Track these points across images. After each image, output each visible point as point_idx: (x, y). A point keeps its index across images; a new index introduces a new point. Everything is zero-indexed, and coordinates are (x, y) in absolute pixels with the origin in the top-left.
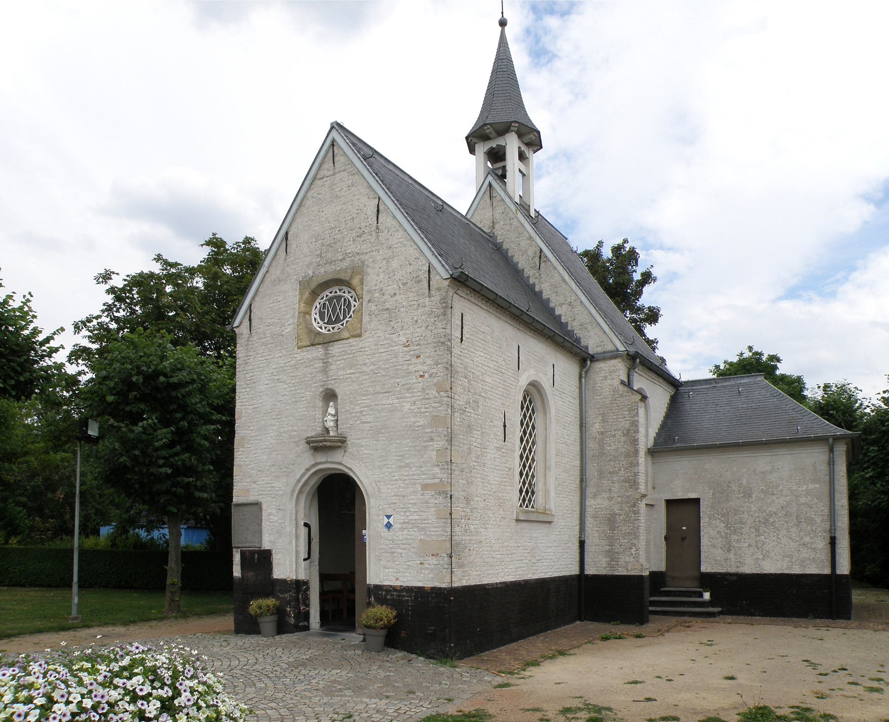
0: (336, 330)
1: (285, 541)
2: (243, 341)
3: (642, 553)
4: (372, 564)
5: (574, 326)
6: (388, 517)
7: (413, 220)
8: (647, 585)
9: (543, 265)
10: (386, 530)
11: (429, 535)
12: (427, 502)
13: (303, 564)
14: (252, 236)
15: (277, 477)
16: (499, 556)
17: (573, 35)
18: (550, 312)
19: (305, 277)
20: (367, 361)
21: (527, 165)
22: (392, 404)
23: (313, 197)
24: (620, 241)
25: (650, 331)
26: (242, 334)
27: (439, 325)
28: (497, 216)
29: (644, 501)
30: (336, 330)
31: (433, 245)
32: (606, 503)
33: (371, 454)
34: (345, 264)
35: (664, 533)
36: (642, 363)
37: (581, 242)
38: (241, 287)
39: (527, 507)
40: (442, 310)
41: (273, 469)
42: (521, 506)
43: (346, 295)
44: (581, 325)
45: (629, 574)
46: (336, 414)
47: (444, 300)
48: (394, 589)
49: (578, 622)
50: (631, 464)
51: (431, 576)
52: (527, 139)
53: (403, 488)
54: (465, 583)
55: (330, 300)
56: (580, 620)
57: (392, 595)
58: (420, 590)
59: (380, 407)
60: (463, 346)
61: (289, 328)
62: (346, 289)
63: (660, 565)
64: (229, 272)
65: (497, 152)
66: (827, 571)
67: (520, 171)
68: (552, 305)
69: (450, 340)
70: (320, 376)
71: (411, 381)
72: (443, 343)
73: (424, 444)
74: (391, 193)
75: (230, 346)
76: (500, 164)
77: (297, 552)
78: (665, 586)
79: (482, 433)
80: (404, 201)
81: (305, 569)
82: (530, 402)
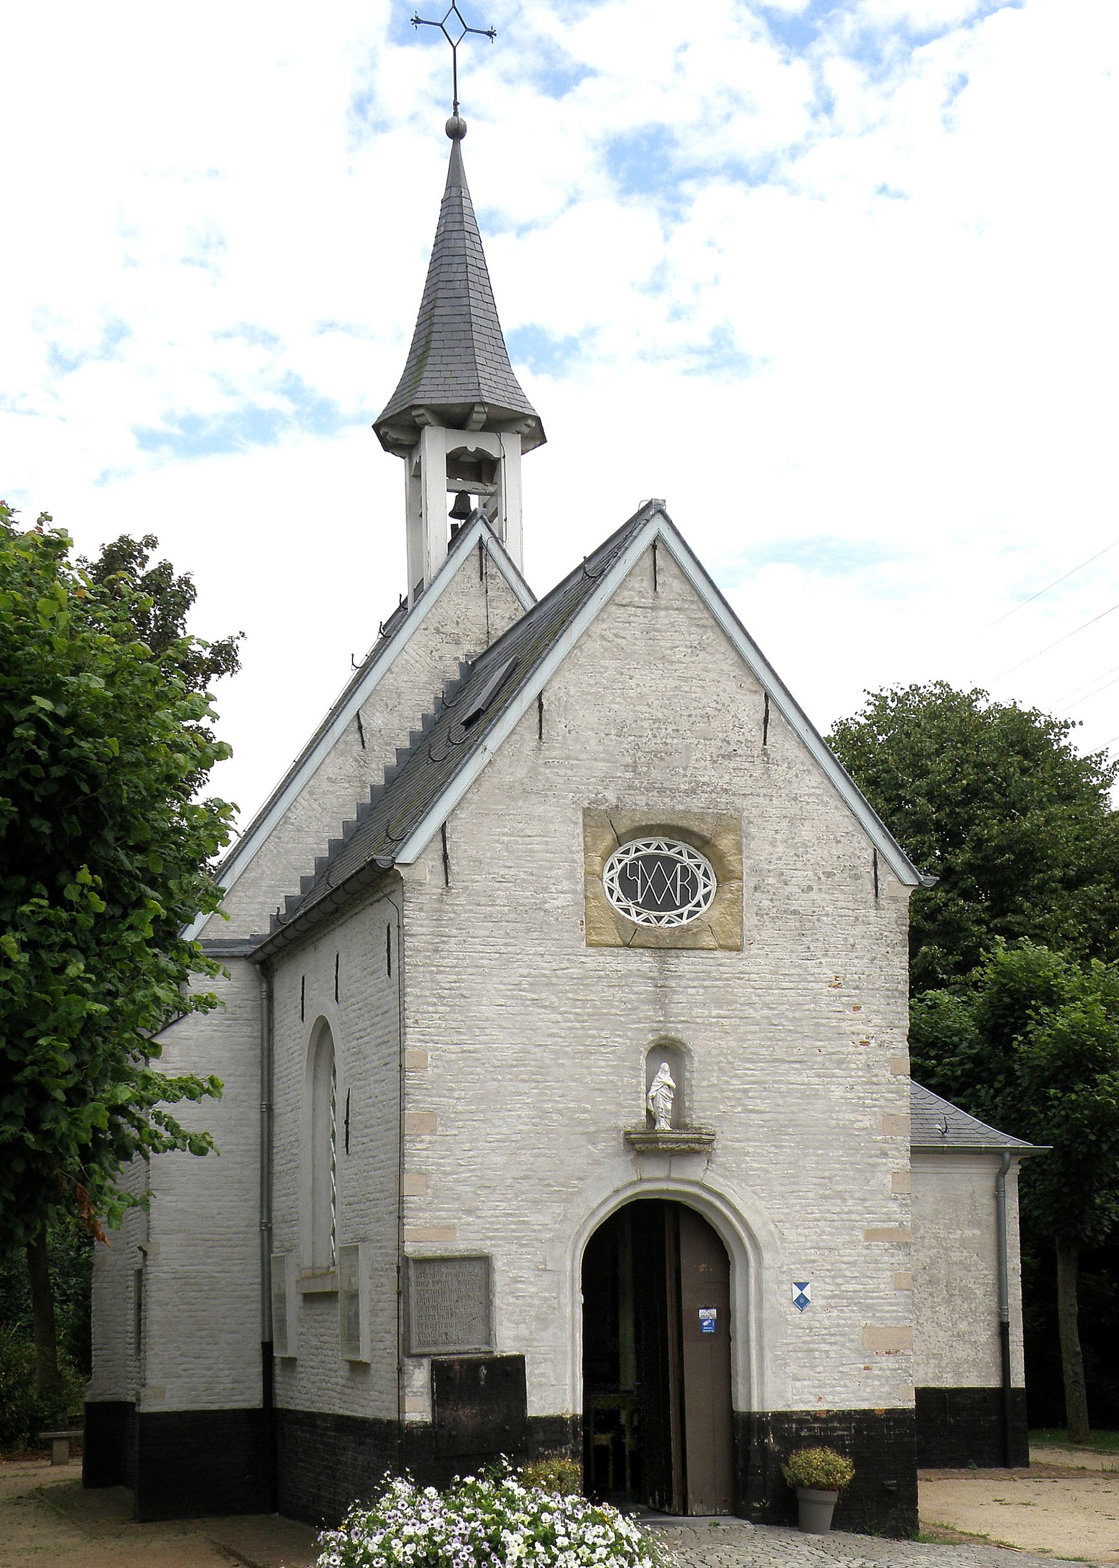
6: (801, 1286)
10: (794, 1309)
11: (880, 1319)
12: (876, 1262)
15: (535, 1202)
20: (755, 999)
22: (809, 1084)
23: (603, 637)
33: (768, 1172)
41: (525, 1185)
48: (815, 1417)
51: (886, 1389)
53: (830, 1234)
55: (649, 860)
57: (810, 1429)
59: (783, 1088)
66: (994, 1383)
70: (648, 1011)
73: (870, 1161)
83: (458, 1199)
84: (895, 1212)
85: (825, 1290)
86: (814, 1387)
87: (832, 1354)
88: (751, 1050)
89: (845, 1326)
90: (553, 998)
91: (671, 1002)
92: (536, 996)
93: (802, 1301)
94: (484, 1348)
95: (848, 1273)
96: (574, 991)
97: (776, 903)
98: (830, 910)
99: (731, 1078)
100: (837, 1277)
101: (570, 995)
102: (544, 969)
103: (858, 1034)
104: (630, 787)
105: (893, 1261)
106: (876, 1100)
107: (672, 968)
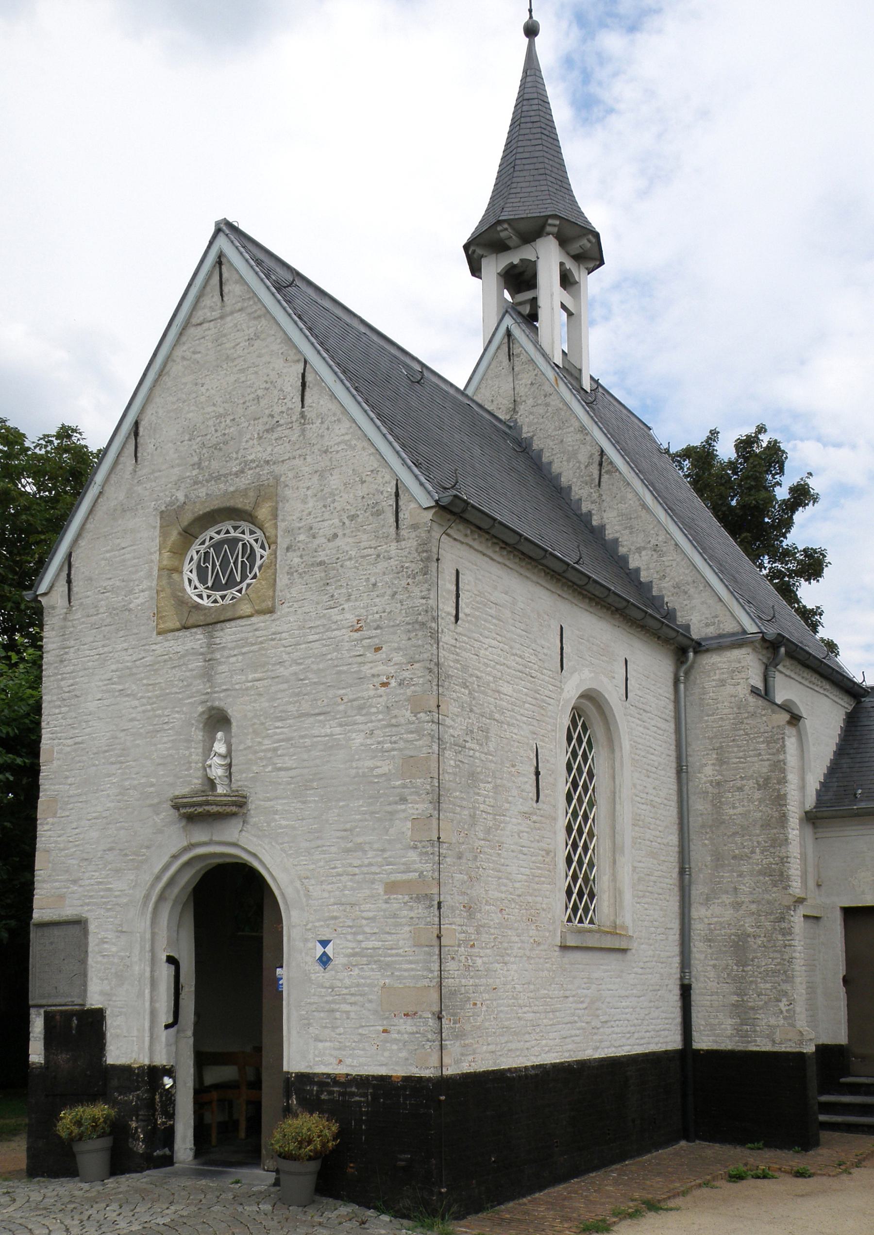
0: (227, 601)
1: (129, 990)
2: (55, 620)
3: (800, 1008)
4: (294, 1032)
5: (664, 589)
6: (324, 943)
7: (367, 402)
8: (812, 1071)
9: (605, 477)
10: (319, 968)
11: (399, 978)
12: (395, 916)
13: (163, 1035)
14: (73, 425)
15: (117, 871)
16: (530, 1016)
17: (653, 62)
18: (620, 563)
19: (171, 503)
21: (576, 296)
22: (332, 735)
24: (751, 430)
25: (808, 593)
26: (53, 608)
27: (416, 591)
28: (522, 390)
29: (802, 911)
30: (227, 601)
31: (403, 446)
32: (729, 914)
33: (293, 828)
34: (243, 482)
35: (841, 971)
36: (790, 655)
37: (676, 432)
38: (53, 519)
39: (581, 921)
40: (421, 565)
42: (569, 920)
43: (247, 537)
44: (677, 586)
45: (776, 1049)
46: (229, 755)
47: (423, 546)
49: (683, 1143)
50: (774, 840)
51: (403, 1054)
52: (575, 248)
53: (352, 889)
54: (467, 1067)
55: (218, 546)
56: (688, 1140)
57: (331, 1093)
58: (383, 1081)
60: (459, 630)
61: (143, 595)
62: (245, 526)
63: (837, 1033)
64: (30, 489)
65: (521, 274)
67: (563, 307)
68: (622, 550)
69: (435, 619)
70: (199, 685)
71: (365, 694)
72: (423, 624)
73: (389, 808)
74: (327, 350)
75: (32, 625)
76: (527, 295)
77: (153, 1013)
78: (849, 1075)
79: (496, 787)
80: (351, 367)
81: (168, 1045)
82: (585, 728)
83: (67, 871)
84: (414, 862)
85: (347, 948)
86: (335, 1049)
87: (352, 1015)
88: (281, 708)
89: (364, 985)
90: (134, 687)
91: (216, 674)
92: (121, 687)
93: (324, 959)
94: (78, 1001)
95: (367, 930)
96: (148, 678)
97: (305, 558)
98: (353, 553)
99: (263, 738)
100: (358, 934)
101: (145, 682)
102: (128, 662)
103: (379, 675)
104: (196, 483)
105: (412, 914)
106: (395, 742)
107: (218, 641)
